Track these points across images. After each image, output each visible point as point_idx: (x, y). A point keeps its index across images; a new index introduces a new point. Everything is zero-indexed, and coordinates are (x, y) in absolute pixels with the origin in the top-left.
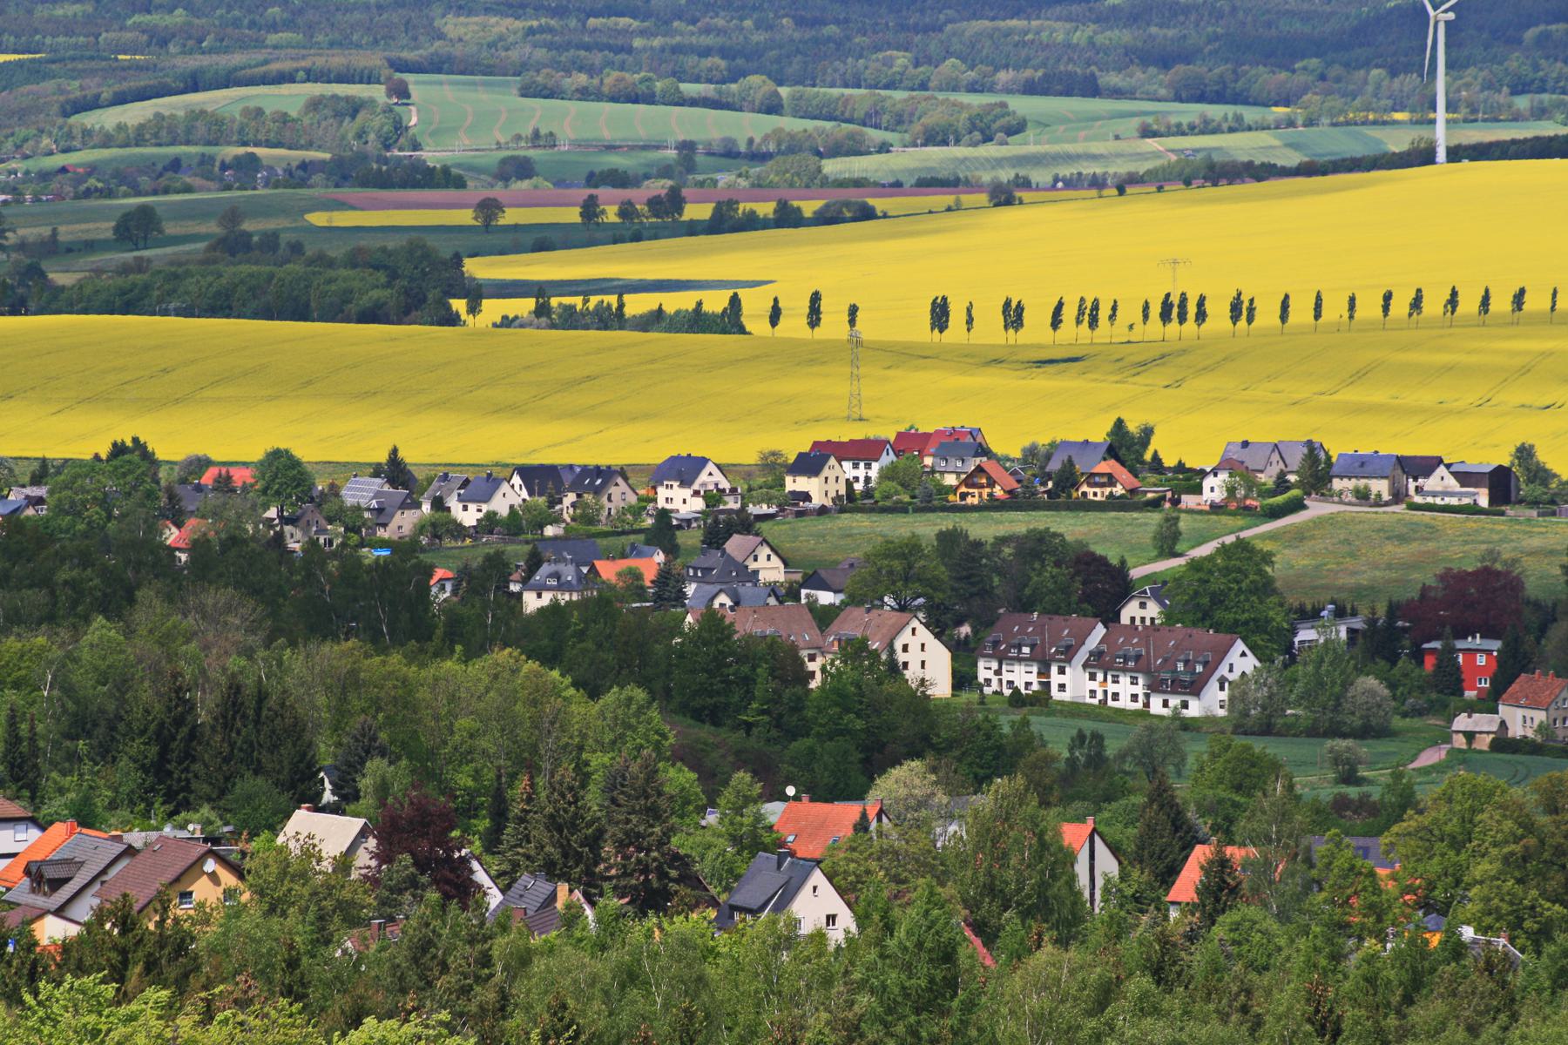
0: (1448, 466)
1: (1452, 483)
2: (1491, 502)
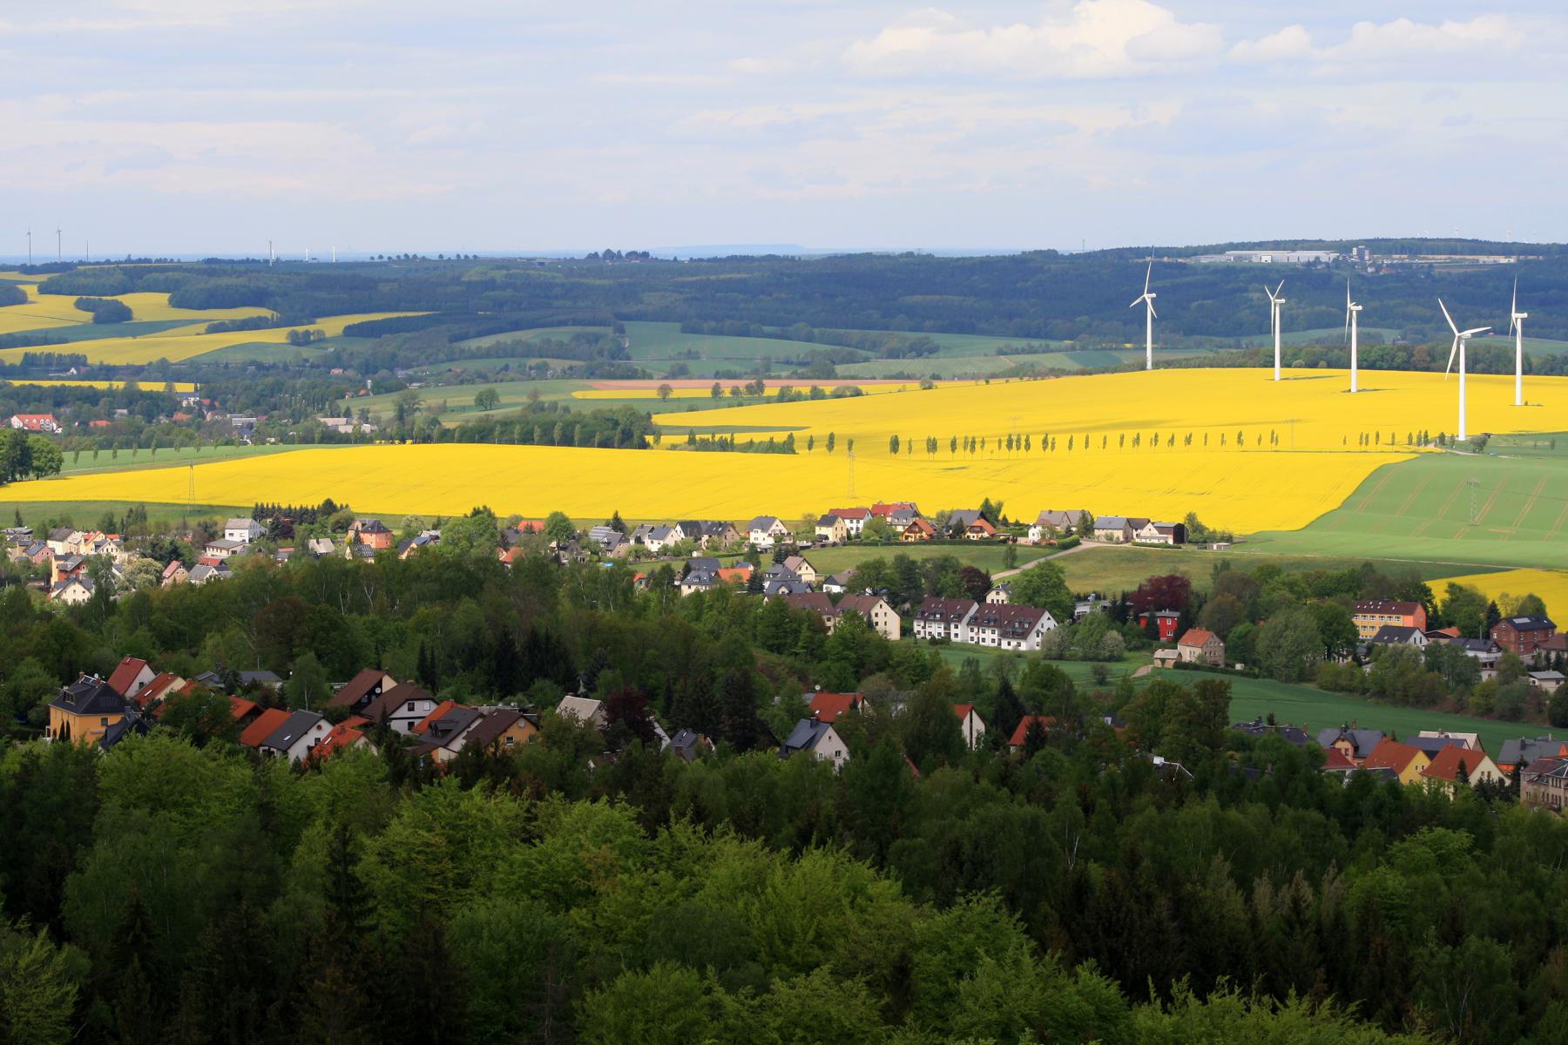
0: (1153, 524)
1: (1155, 532)
2: (1174, 542)
